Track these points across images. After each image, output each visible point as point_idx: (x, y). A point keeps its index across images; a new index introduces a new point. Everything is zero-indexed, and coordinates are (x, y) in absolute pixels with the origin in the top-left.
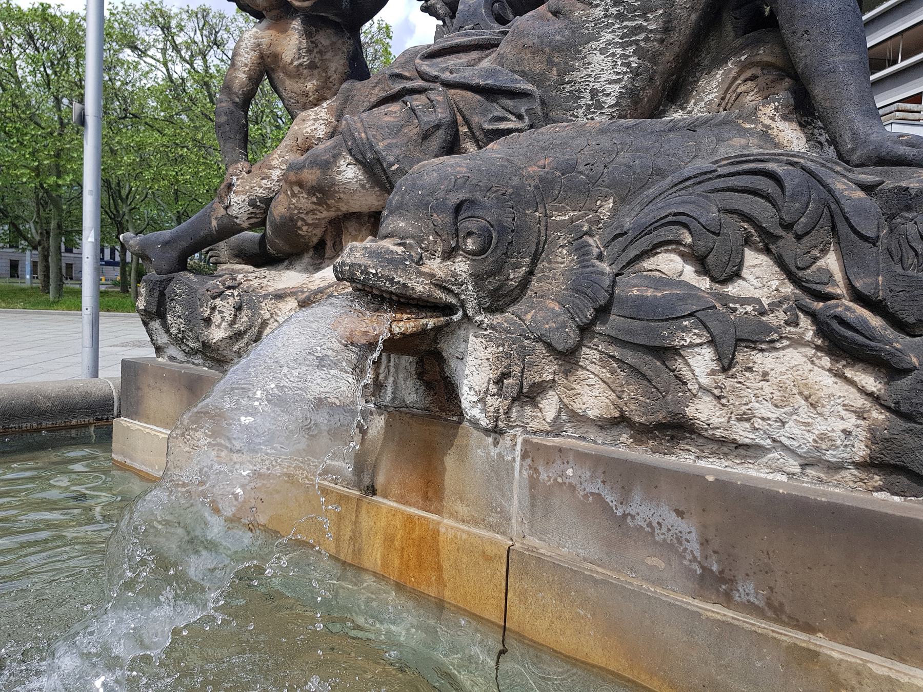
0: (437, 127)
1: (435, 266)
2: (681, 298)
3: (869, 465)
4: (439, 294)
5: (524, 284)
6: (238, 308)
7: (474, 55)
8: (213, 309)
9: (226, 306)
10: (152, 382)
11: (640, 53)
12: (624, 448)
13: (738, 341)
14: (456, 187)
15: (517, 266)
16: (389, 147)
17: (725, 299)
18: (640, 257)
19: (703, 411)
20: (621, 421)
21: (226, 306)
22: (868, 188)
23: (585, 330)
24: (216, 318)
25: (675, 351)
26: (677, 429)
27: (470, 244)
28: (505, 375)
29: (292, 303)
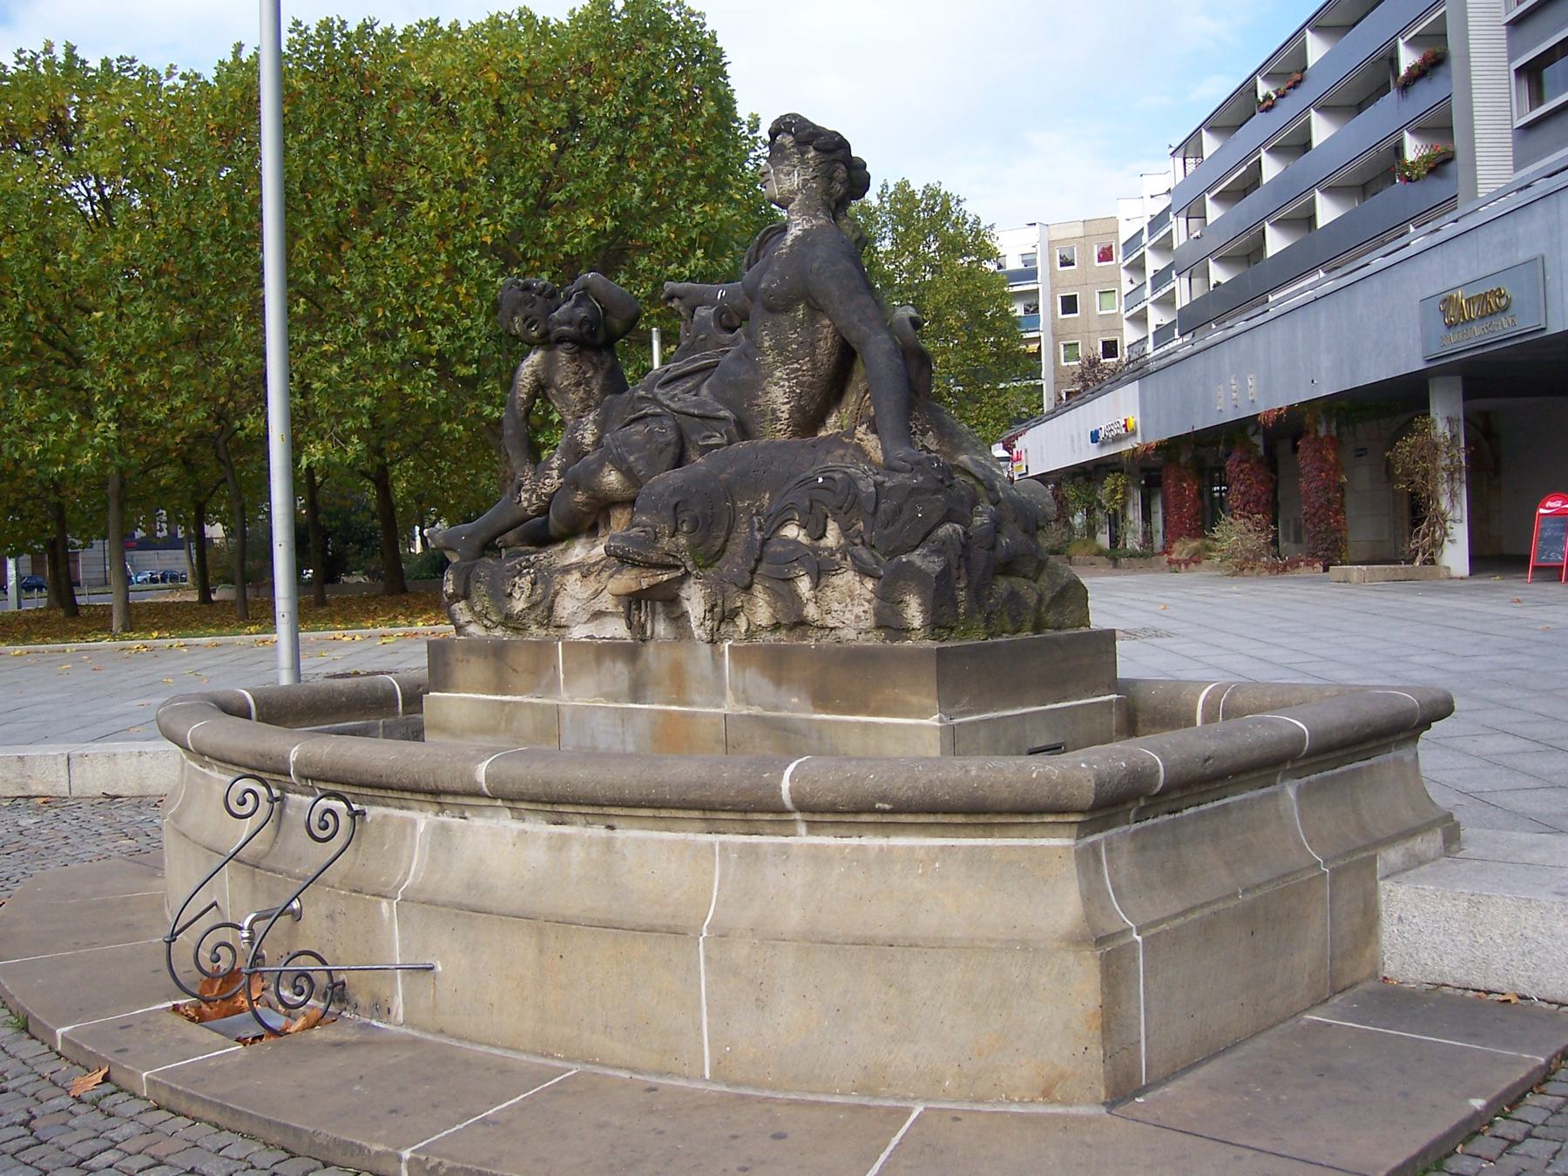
0: (668, 444)
3: (879, 627)
5: (722, 550)
6: (534, 583)
7: (698, 378)
10: (460, 656)
13: (821, 572)
14: (675, 492)
15: (717, 538)
16: (636, 460)
19: (811, 611)
20: (776, 627)
24: (516, 595)
29: (576, 575)
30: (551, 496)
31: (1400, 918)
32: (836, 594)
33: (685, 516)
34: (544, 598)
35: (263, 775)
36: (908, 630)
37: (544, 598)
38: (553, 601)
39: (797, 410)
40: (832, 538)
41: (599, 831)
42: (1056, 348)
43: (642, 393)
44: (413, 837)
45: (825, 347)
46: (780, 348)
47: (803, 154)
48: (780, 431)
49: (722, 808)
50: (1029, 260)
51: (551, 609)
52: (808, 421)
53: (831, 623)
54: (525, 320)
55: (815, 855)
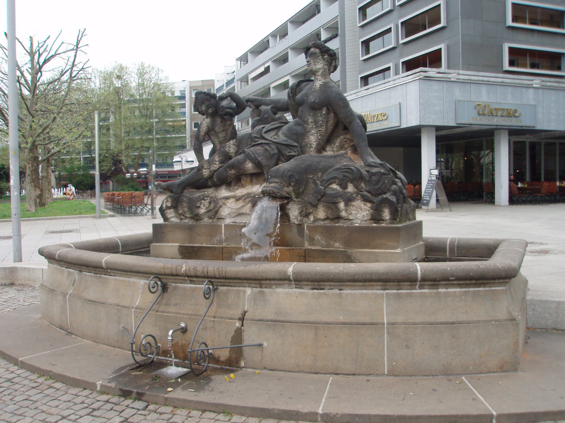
0: (275, 154)
1: (285, 189)
2: (338, 193)
3: (371, 219)
4: (287, 195)
5: (303, 192)
6: (210, 203)
8: (201, 203)
9: (206, 203)
11: (320, 135)
12: (327, 223)
13: (349, 201)
15: (302, 188)
16: (262, 159)
17: (345, 193)
18: (328, 185)
19: (343, 214)
20: (327, 218)
21: (206, 203)
22: (368, 171)
23: (319, 200)
24: (202, 206)
25: (337, 203)
26: (338, 218)
27: (293, 184)
28: (301, 212)
30: (215, 171)
31: (533, 310)
32: (354, 208)
33: (293, 180)
34: (215, 208)
35: (160, 277)
36: (383, 220)
37: (215, 208)
38: (218, 210)
39: (318, 144)
40: (351, 188)
41: (336, 291)
42: (191, 124)
43: (256, 135)
44: (244, 296)
45: (331, 122)
46: (316, 122)
47: (323, 56)
48: (312, 151)
49: (404, 281)
50: (183, 92)
51: (217, 212)
52: (321, 148)
53: (351, 217)
54: (207, 106)
55: (423, 296)
